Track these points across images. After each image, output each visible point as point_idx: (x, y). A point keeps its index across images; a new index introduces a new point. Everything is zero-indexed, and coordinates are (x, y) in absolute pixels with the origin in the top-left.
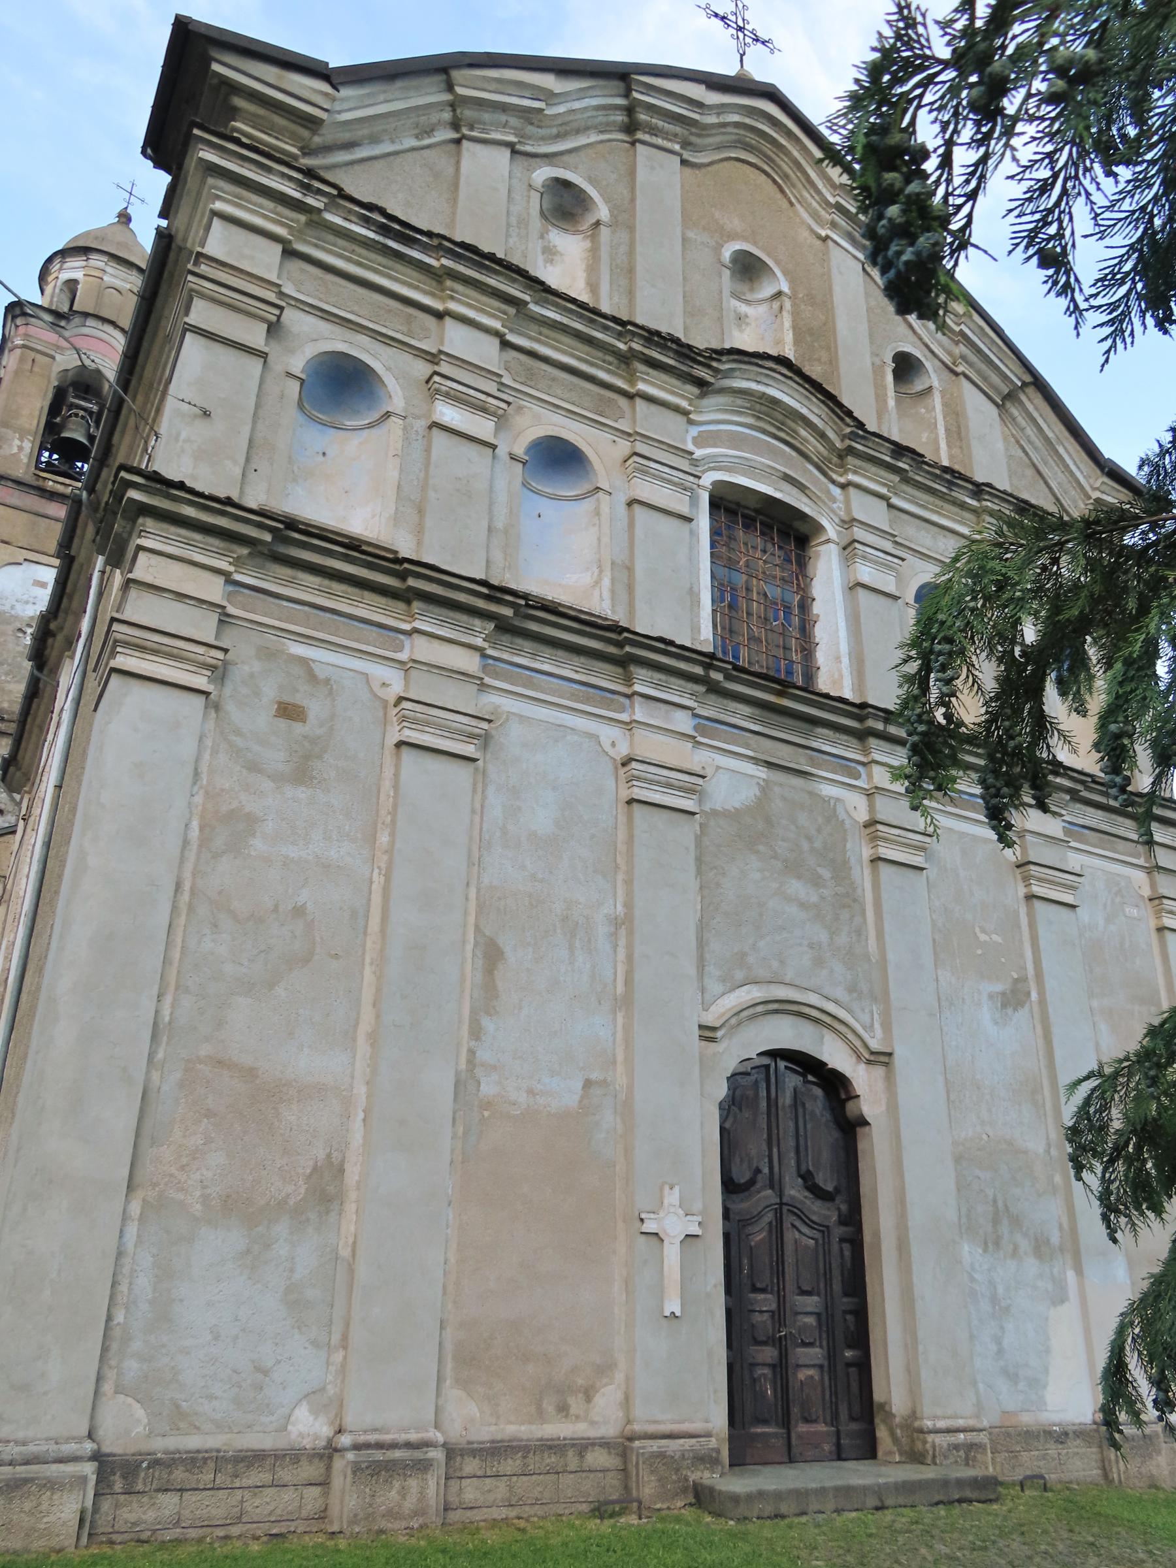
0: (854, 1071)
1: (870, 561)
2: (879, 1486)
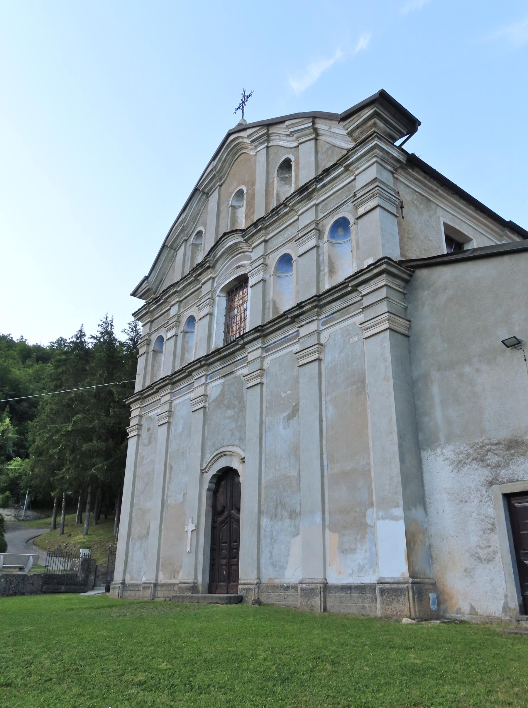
1: (254, 275)
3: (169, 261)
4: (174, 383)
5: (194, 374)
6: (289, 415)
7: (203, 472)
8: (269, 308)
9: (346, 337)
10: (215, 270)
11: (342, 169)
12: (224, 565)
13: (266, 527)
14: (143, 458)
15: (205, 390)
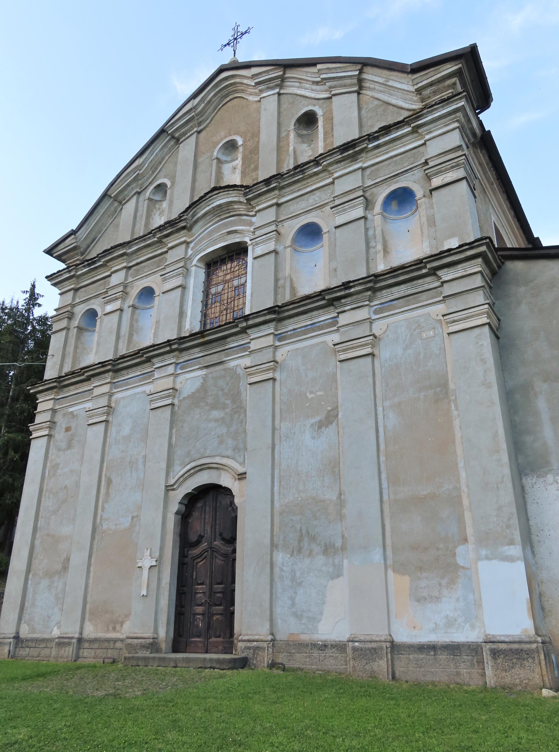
0: (233, 485)
2: (176, 658)
3: (109, 216)
4: (117, 371)
5: (155, 360)
6: (320, 421)
7: (169, 488)
8: (284, 287)
9: (415, 330)
10: (190, 233)
11: (408, 129)
12: (199, 614)
13: (283, 564)
14: (56, 466)
15: (174, 382)
